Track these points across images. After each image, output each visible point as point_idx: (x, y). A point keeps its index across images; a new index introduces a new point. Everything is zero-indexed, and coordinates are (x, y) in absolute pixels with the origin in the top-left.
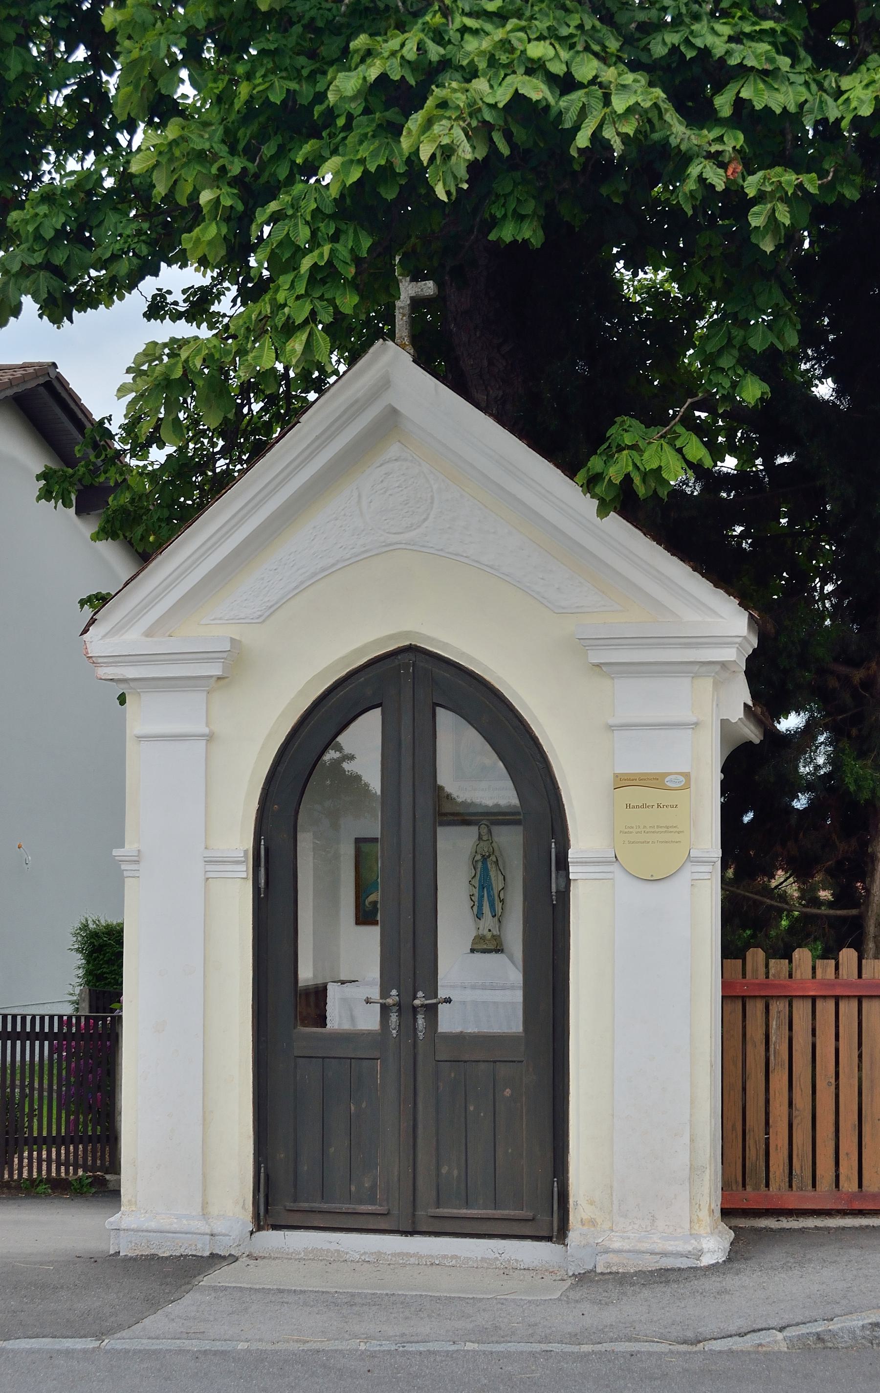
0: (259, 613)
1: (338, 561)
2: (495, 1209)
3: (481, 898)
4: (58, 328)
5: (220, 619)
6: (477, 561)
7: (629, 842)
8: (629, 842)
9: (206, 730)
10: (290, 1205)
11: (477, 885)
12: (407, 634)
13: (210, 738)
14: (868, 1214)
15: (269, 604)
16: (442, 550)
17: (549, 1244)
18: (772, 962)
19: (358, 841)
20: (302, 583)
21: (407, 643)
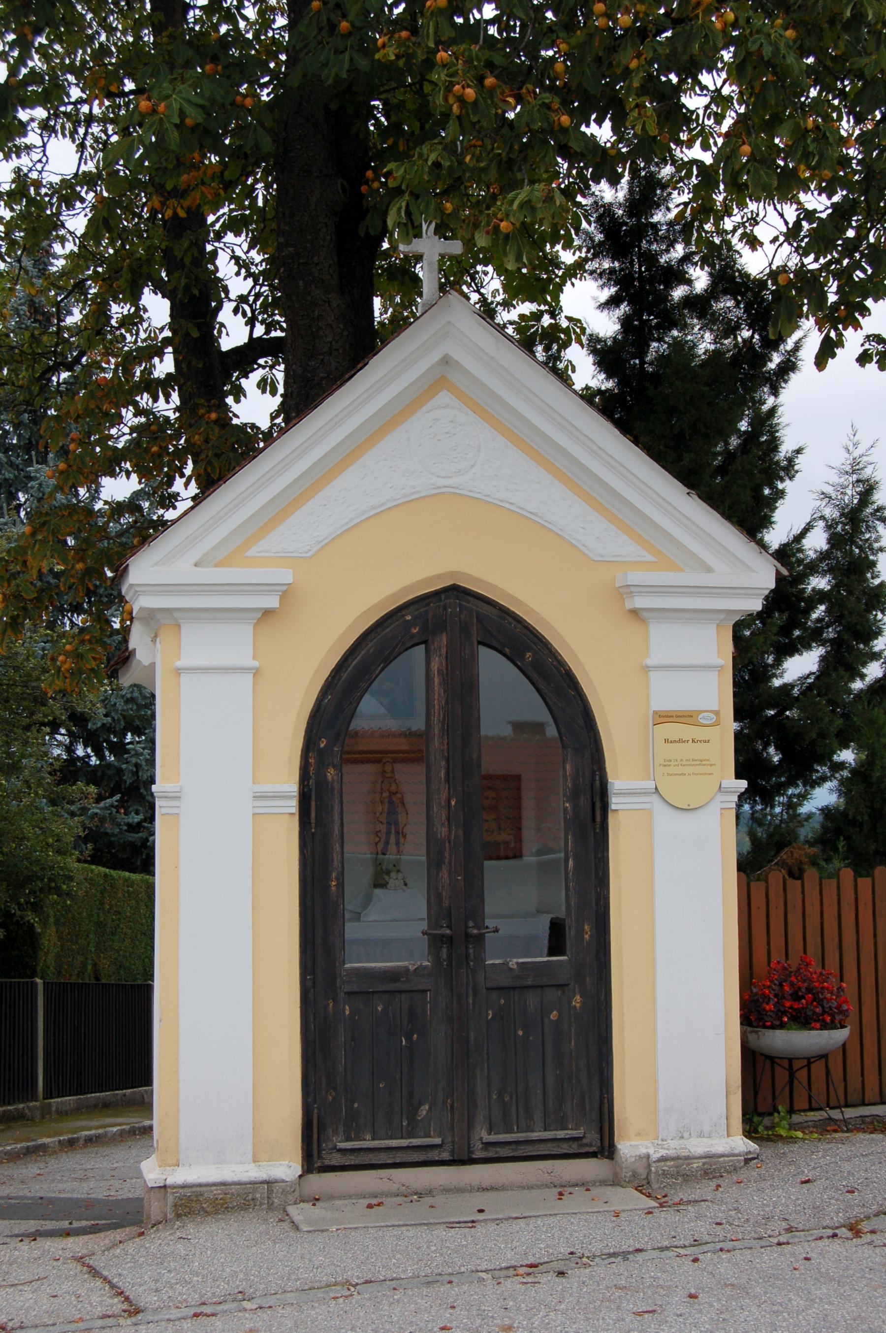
0: (309, 548)
1: (388, 501)
2: (545, 1130)
3: (388, 833)
4: (861, 329)
5: (268, 551)
6: (522, 509)
7: (668, 774)
8: (668, 774)
9: (256, 664)
10: (487, 1138)
11: (385, 821)
12: (453, 574)
13: (257, 673)
14: (308, 1146)
15: (320, 539)
16: (488, 496)
17: (595, 1159)
18: (859, 880)
19: (518, 778)
20: (352, 520)
21: (452, 583)
